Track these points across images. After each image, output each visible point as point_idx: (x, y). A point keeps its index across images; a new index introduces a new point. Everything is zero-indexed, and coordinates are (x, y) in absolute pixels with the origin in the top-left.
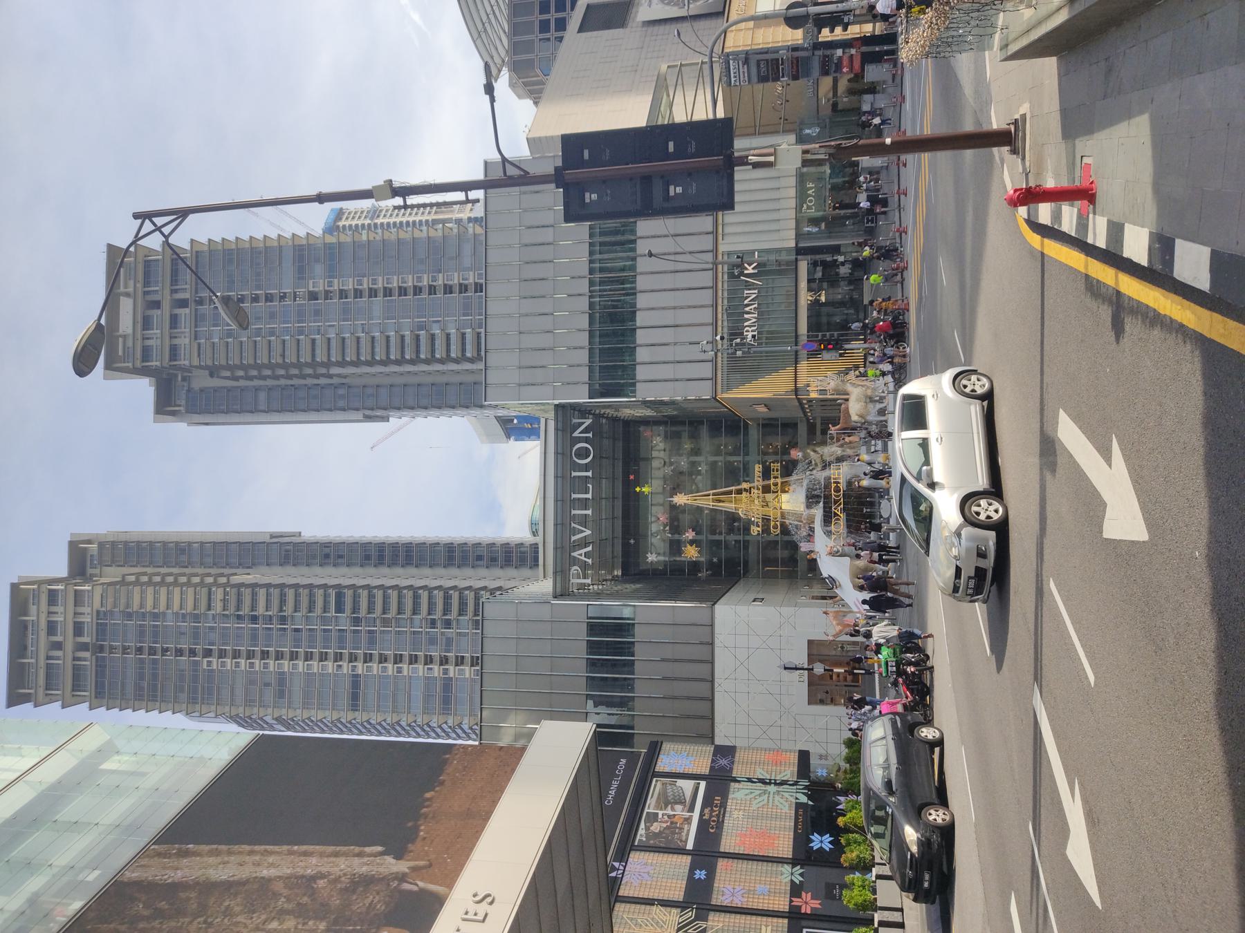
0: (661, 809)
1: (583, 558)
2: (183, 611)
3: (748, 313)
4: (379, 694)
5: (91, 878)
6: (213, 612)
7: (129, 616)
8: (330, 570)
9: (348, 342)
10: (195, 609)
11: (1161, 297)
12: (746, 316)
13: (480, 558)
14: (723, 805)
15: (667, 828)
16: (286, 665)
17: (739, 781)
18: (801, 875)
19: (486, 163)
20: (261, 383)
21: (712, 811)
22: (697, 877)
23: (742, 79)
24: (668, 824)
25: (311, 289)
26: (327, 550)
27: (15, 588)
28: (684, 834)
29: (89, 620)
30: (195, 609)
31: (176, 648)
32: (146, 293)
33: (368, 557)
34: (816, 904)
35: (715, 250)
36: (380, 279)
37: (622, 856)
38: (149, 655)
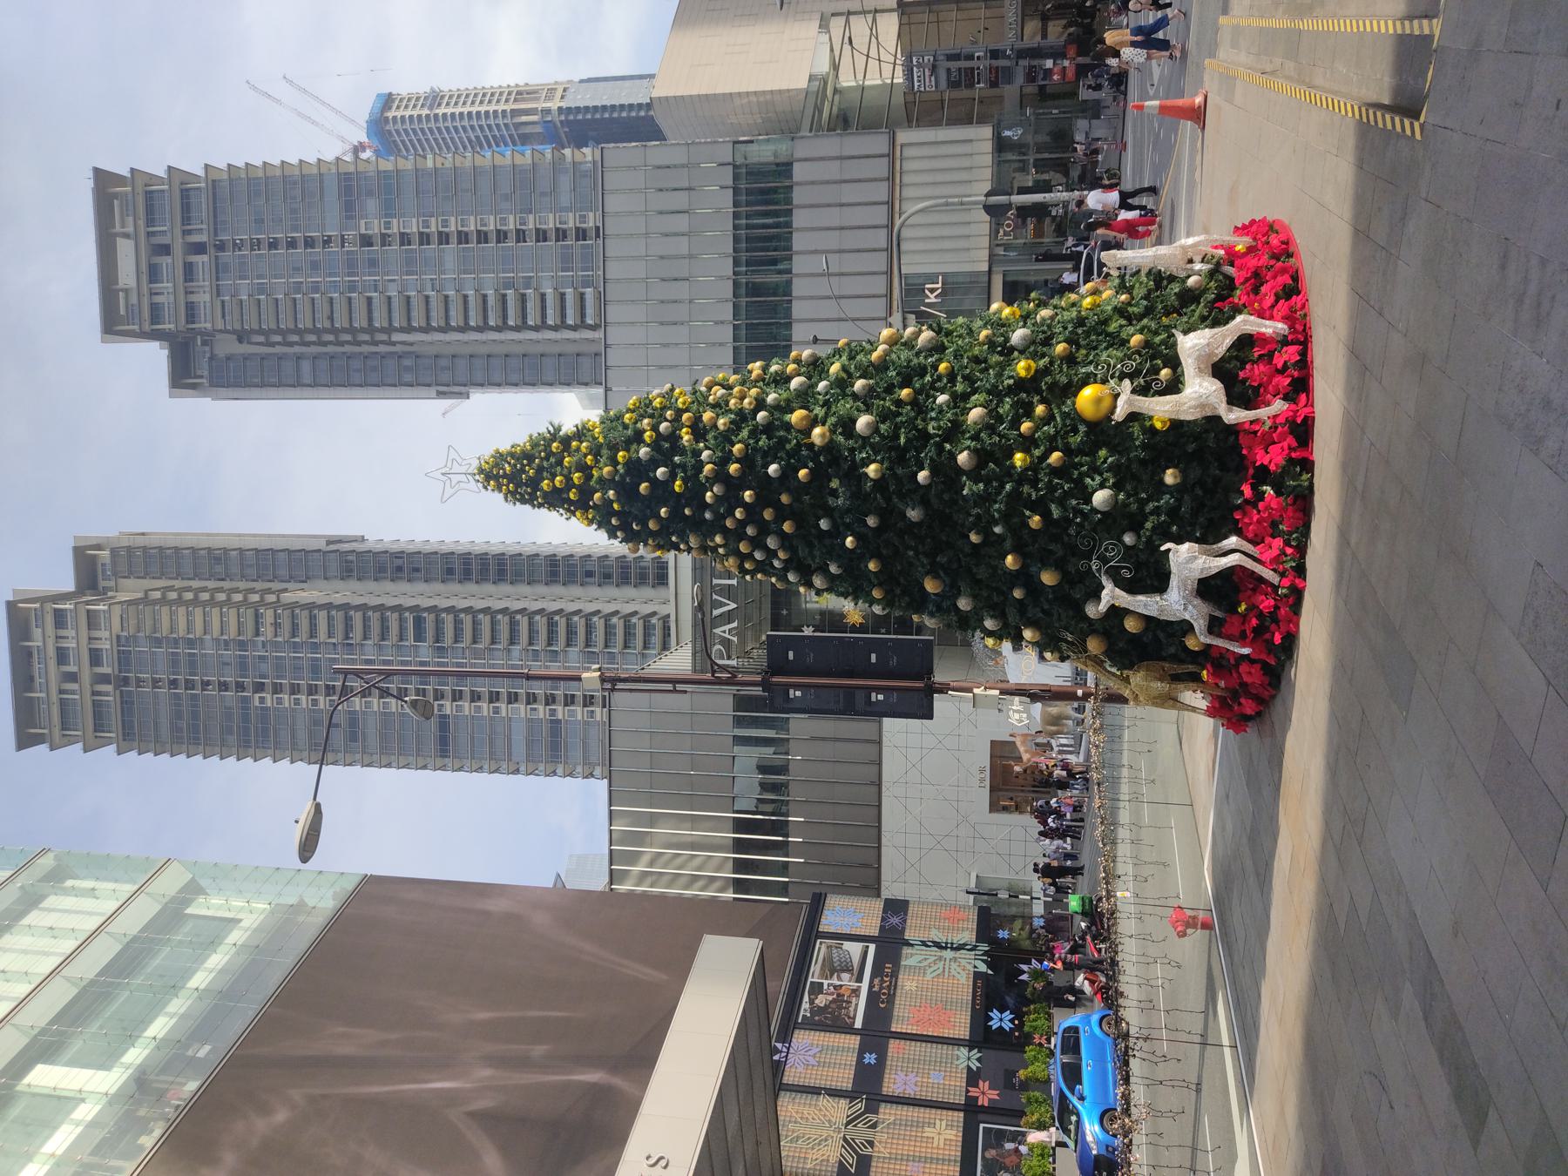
0: (826, 979)
1: (727, 635)
2: (226, 637)
4: (472, 738)
5: (202, 1054)
6: (262, 639)
7: (158, 642)
8: (404, 586)
9: (414, 302)
10: (239, 635)
13: (589, 574)
14: (895, 974)
15: (834, 1001)
16: (357, 703)
17: (912, 945)
18: (979, 1060)
20: (304, 349)
21: (882, 981)
22: (866, 1061)
23: (927, 84)
25: (363, 231)
26: (399, 562)
27: (11, 606)
28: (852, 1009)
29: (108, 647)
30: (239, 635)
31: (219, 681)
32: (149, 234)
33: (450, 571)
34: (993, 1095)
36: (453, 219)
37: (785, 1035)
38: (186, 689)
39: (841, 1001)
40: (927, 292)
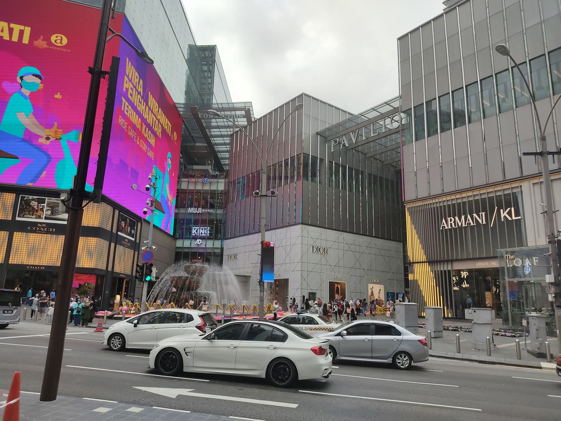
3: (466, 218)
11: (203, 284)
12: (463, 217)
14: (47, 232)
15: (33, 208)
21: (44, 228)
28: (29, 216)
35: (523, 178)
39: (32, 211)
40: (509, 209)
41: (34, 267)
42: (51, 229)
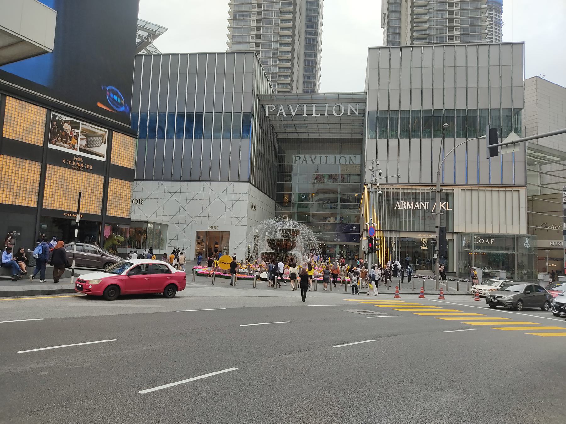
0: (81, 132)
1: (279, 111)
12: (413, 203)
13: (308, 78)
14: (85, 170)
19: (522, 43)
21: (80, 163)
24: (70, 135)
28: (62, 143)
35: (455, 185)
39: (66, 138)
40: (445, 203)
41: (71, 215)
42: (88, 165)
